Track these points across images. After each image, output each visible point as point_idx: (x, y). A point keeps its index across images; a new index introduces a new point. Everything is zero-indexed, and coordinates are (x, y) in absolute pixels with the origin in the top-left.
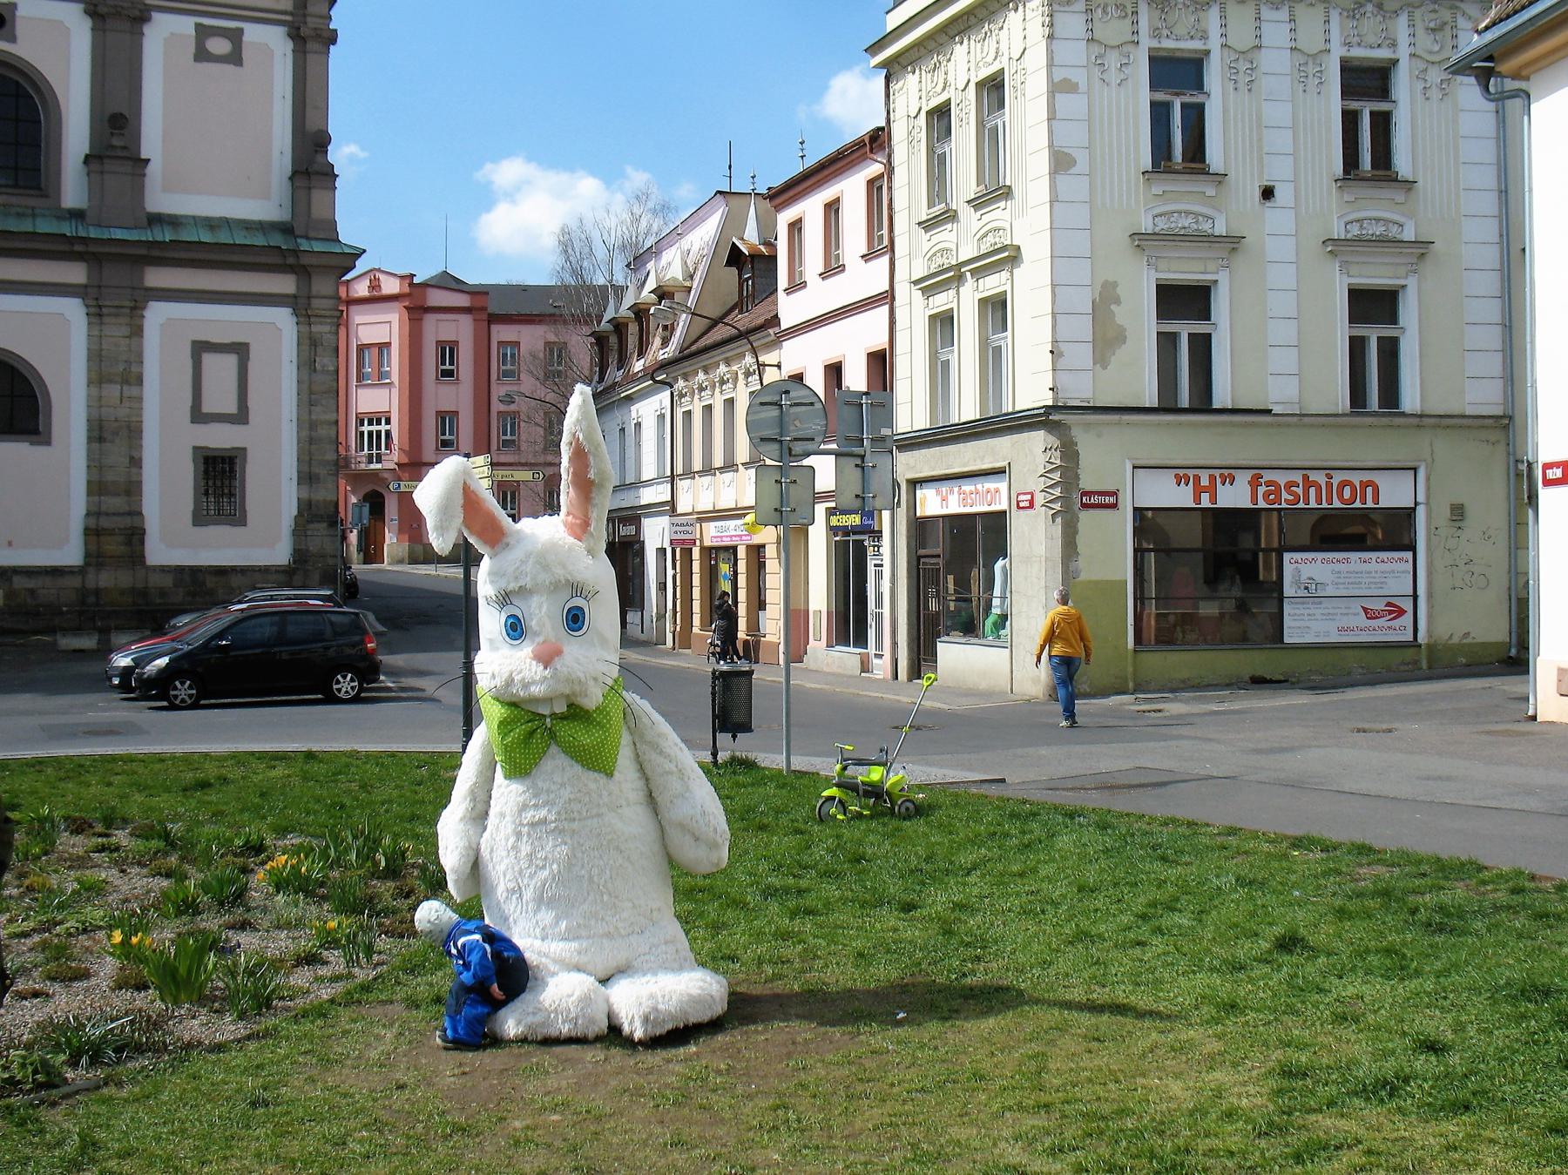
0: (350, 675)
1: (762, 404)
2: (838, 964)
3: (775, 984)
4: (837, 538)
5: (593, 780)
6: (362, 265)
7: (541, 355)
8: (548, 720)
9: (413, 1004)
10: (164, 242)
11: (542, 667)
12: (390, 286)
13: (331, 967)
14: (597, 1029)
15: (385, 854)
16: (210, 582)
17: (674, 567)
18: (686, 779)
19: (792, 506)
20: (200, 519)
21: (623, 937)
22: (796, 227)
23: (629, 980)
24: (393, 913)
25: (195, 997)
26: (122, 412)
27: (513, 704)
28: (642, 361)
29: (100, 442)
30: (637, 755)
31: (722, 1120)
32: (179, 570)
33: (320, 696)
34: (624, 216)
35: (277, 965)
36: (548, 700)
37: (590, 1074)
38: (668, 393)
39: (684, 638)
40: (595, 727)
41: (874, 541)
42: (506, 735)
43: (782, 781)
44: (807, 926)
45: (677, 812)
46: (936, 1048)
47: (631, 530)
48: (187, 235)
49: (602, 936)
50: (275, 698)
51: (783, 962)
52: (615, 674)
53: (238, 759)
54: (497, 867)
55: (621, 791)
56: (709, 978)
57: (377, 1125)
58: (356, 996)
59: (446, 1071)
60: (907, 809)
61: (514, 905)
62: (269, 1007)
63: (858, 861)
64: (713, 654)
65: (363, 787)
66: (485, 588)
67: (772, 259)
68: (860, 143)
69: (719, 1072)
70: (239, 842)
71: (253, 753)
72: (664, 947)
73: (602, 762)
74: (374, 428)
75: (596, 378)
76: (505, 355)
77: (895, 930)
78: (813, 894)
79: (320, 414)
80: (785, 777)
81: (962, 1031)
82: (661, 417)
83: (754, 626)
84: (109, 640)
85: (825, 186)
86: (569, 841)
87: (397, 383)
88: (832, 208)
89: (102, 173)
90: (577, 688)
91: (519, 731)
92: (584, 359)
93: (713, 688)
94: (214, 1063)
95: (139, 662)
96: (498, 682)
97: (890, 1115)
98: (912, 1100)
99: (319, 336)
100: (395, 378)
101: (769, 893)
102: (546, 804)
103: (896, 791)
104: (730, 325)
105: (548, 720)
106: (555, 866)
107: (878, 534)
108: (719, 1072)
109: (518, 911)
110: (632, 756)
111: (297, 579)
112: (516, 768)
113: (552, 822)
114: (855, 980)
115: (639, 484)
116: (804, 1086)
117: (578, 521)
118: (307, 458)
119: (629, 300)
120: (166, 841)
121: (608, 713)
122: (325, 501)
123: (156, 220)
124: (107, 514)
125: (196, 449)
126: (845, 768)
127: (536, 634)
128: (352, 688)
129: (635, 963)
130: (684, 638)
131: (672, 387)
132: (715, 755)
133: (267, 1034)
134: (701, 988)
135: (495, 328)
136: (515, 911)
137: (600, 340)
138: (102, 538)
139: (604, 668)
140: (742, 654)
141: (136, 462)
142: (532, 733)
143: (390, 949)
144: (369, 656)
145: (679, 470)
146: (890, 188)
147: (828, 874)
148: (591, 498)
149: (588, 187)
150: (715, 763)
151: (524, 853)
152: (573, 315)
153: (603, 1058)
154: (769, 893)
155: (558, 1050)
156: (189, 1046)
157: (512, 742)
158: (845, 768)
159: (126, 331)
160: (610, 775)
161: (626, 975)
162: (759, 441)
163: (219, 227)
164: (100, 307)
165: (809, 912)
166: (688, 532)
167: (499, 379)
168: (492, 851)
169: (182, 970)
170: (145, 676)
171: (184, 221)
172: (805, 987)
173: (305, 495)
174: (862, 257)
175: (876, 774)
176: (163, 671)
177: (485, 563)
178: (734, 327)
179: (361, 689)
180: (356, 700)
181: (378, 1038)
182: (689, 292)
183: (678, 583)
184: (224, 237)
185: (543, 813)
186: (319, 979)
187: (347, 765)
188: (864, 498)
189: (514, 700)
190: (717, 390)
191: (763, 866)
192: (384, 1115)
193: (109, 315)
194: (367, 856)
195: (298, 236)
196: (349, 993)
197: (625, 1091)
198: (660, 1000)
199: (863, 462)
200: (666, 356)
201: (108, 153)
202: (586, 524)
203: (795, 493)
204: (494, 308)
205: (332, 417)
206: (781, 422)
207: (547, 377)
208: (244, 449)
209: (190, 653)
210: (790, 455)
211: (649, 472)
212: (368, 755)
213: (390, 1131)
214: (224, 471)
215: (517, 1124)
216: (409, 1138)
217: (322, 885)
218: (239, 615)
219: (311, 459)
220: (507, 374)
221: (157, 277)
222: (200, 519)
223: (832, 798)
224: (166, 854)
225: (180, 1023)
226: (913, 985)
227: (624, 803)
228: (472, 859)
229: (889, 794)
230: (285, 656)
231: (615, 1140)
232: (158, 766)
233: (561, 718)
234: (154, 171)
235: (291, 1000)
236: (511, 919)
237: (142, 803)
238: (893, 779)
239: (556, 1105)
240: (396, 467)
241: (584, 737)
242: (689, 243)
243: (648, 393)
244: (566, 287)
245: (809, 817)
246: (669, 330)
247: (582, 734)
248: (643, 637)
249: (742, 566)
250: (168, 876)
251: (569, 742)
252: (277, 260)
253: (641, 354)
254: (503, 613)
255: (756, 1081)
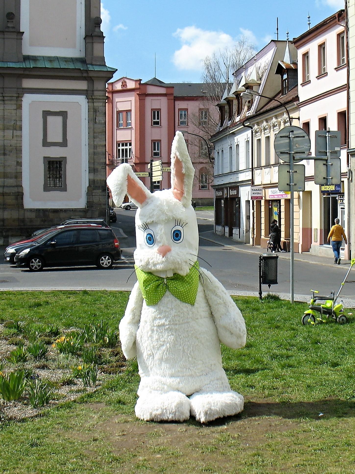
0: (40, 264)
1: (281, 137)
2: (298, 390)
3: (268, 398)
4: (325, 196)
5: (185, 307)
6: (116, 77)
7: (197, 115)
8: (165, 280)
9: (109, 403)
10: (30, 68)
11: (162, 257)
12: (131, 85)
13: (78, 386)
14: (184, 417)
15: (108, 337)
16: (51, 215)
17: (253, 209)
18: (227, 307)
19: (295, 182)
20: (46, 188)
21: (198, 377)
22: (306, 56)
23: (200, 395)
24: (109, 363)
25: (17, 398)
26: (13, 142)
27: (150, 273)
28: (239, 117)
29: (4, 155)
30: (206, 296)
31: (230, 460)
32: (38, 210)
33: (95, 266)
34: (234, 52)
35: (51, 385)
36: (164, 271)
37: (178, 437)
38: (250, 131)
39: (258, 241)
40: (186, 283)
41: (341, 197)
42: (146, 286)
43: (289, 306)
44: (288, 372)
45: (222, 322)
46: (332, 430)
47: (234, 192)
48: (40, 65)
49: (189, 376)
50: (53, 268)
51: (274, 389)
52: (195, 259)
53: (54, 293)
54: (143, 345)
55: (198, 312)
56: (235, 396)
57: (81, 457)
58: (85, 399)
59: (116, 433)
60: (343, 320)
61: (150, 361)
62: (47, 403)
63: (316, 343)
64: (270, 248)
65: (106, 306)
66: (138, 223)
67: (296, 70)
68: (333, 17)
69: (234, 438)
70: (48, 330)
71: (61, 291)
72: (216, 381)
73: (189, 299)
74: (124, 148)
75: (220, 125)
76: (181, 115)
77: (328, 375)
78: (294, 358)
79: (98, 142)
80: (291, 304)
81: (347, 423)
82: (248, 142)
83: (288, 236)
84: (8, 241)
85: (322, 35)
86: (174, 334)
87: (134, 128)
88: (322, 47)
89: (4, 38)
90: (177, 266)
91: (153, 285)
92: (216, 116)
93: (260, 264)
94: (20, 427)
95: (18, 251)
96: (143, 263)
97: (304, 461)
98: (316, 454)
99: (98, 108)
100: (133, 125)
101: (274, 357)
102: (164, 317)
103: (338, 312)
104: (277, 101)
105: (165, 280)
106: (168, 345)
107: (342, 194)
108: (234, 438)
109: (152, 365)
110: (203, 296)
111: (89, 214)
112: (151, 301)
113: (167, 325)
114: (304, 398)
115: (238, 172)
116: (269, 446)
117: (179, 192)
118: (93, 161)
119: (233, 90)
120: (18, 330)
121: (192, 277)
122: (100, 180)
123: (27, 58)
124: (7, 187)
125: (45, 158)
126: (315, 301)
127: (160, 242)
128: (109, 263)
129: (203, 388)
130: (258, 241)
131: (252, 128)
132: (260, 294)
133: (44, 415)
134: (231, 400)
135: (177, 103)
136: (151, 364)
137: (221, 108)
138: (5, 197)
139: (190, 257)
140: (282, 248)
141: (19, 164)
142: (158, 286)
143: (104, 379)
144: (116, 248)
145: (255, 165)
146: (347, 38)
147: (303, 349)
148: (184, 182)
149: (225, 38)
150: (261, 297)
151: (155, 339)
152: (211, 97)
153: (184, 430)
154: (274, 357)
155: (166, 425)
156: (11, 419)
157: (149, 289)
158: (315, 301)
159: (14, 107)
160: (193, 305)
161: (199, 393)
162: (280, 153)
163: (54, 61)
164: (3, 97)
165: (290, 366)
166: (259, 193)
167: (179, 125)
168: (141, 337)
169: (11, 386)
170: (20, 257)
171: (39, 58)
172: (281, 400)
173: (92, 178)
174: (335, 69)
175: (329, 304)
176: (27, 255)
177: (138, 211)
178: (279, 102)
179: (112, 263)
180: (110, 268)
181: (91, 418)
182: (260, 86)
183: (255, 216)
184: (56, 65)
185: (163, 321)
186: (71, 391)
187: (101, 297)
188: (327, 179)
189: (150, 271)
190: (272, 130)
191: (274, 345)
192: (84, 452)
193: (7, 100)
194: (101, 337)
195: (88, 64)
196: (82, 398)
197: (191, 445)
198: (213, 405)
199: (327, 163)
200: (249, 115)
201: (7, 30)
202: (182, 193)
203: (296, 177)
204: (177, 93)
205: (103, 143)
206: (290, 145)
207: (200, 124)
208: (66, 158)
209: (38, 247)
210: (294, 159)
211: (242, 167)
212: (111, 292)
213: (86, 459)
214: (57, 167)
215: (141, 458)
216: (93, 463)
217: (81, 350)
218: (60, 230)
219: (94, 162)
220: (182, 123)
221: (27, 83)
222: (46, 188)
223: (309, 314)
224: (18, 335)
225: (9, 409)
226: (329, 401)
227: (199, 317)
228: (133, 341)
229: (334, 313)
230: (81, 249)
231: (182, 467)
232: (21, 296)
233: (171, 279)
234: (26, 37)
235: (57, 400)
236: (149, 368)
237: (11, 313)
238: (337, 306)
239: (160, 451)
240: (134, 165)
241: (181, 288)
242: (260, 64)
243: (239, 132)
244: (208, 84)
245: (299, 323)
246: (251, 102)
247: (180, 287)
248: (239, 240)
249: (283, 209)
250: (16, 344)
251: (174, 290)
252: (79, 75)
253: (239, 114)
254: (145, 233)
255: (250, 442)
